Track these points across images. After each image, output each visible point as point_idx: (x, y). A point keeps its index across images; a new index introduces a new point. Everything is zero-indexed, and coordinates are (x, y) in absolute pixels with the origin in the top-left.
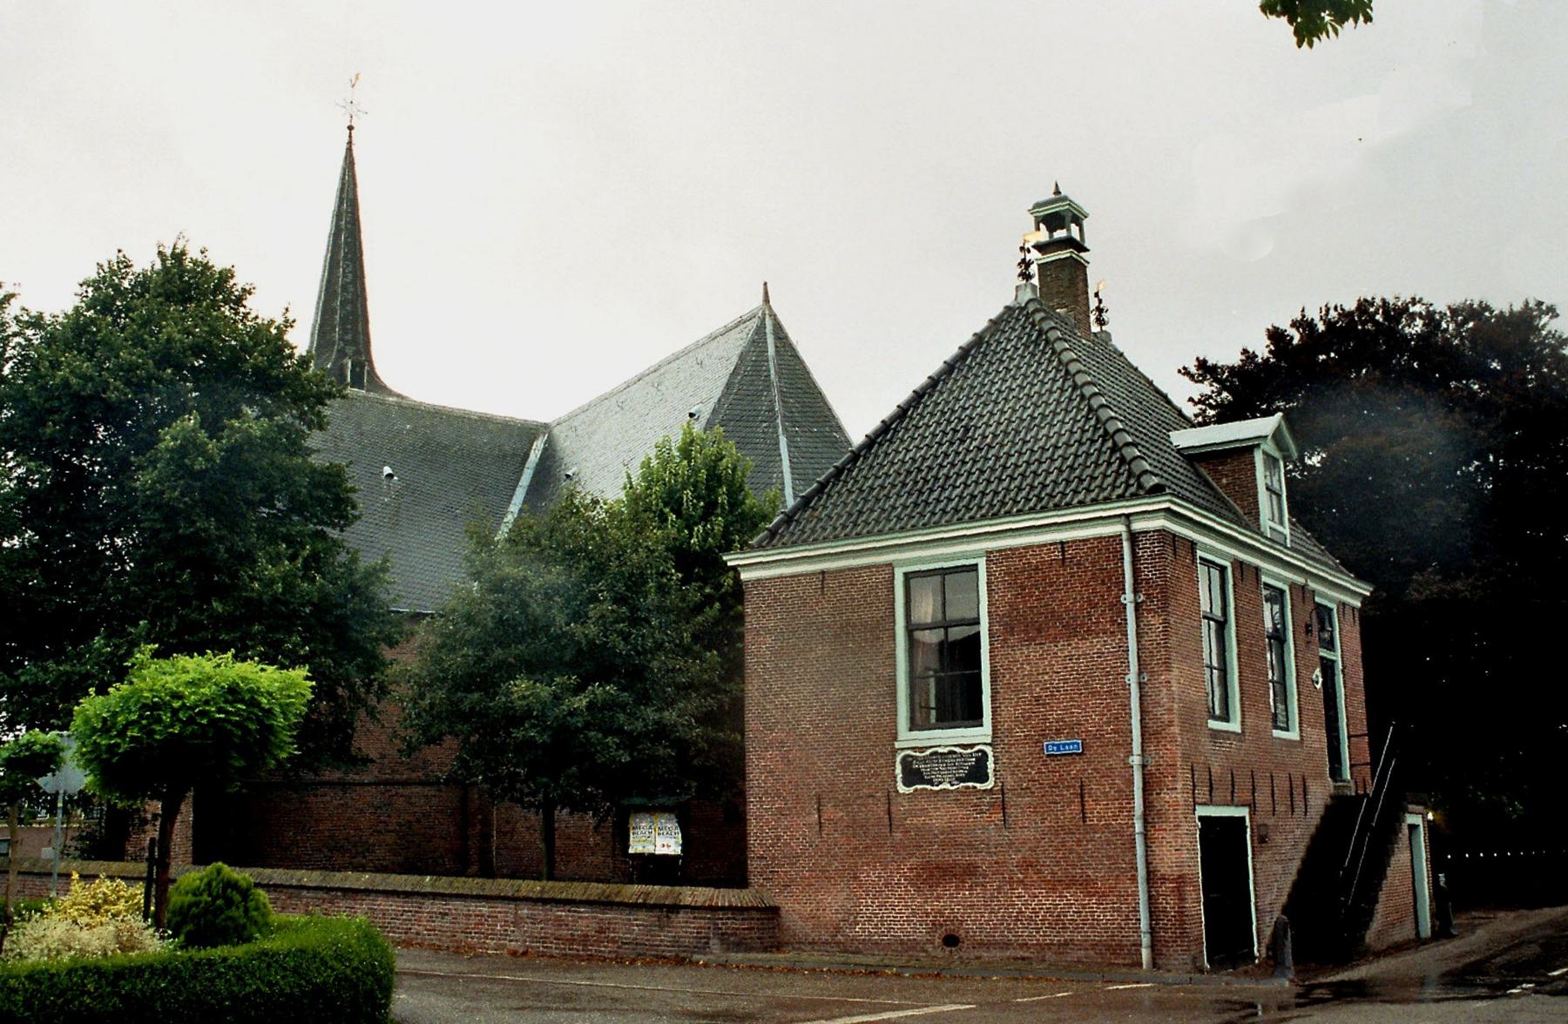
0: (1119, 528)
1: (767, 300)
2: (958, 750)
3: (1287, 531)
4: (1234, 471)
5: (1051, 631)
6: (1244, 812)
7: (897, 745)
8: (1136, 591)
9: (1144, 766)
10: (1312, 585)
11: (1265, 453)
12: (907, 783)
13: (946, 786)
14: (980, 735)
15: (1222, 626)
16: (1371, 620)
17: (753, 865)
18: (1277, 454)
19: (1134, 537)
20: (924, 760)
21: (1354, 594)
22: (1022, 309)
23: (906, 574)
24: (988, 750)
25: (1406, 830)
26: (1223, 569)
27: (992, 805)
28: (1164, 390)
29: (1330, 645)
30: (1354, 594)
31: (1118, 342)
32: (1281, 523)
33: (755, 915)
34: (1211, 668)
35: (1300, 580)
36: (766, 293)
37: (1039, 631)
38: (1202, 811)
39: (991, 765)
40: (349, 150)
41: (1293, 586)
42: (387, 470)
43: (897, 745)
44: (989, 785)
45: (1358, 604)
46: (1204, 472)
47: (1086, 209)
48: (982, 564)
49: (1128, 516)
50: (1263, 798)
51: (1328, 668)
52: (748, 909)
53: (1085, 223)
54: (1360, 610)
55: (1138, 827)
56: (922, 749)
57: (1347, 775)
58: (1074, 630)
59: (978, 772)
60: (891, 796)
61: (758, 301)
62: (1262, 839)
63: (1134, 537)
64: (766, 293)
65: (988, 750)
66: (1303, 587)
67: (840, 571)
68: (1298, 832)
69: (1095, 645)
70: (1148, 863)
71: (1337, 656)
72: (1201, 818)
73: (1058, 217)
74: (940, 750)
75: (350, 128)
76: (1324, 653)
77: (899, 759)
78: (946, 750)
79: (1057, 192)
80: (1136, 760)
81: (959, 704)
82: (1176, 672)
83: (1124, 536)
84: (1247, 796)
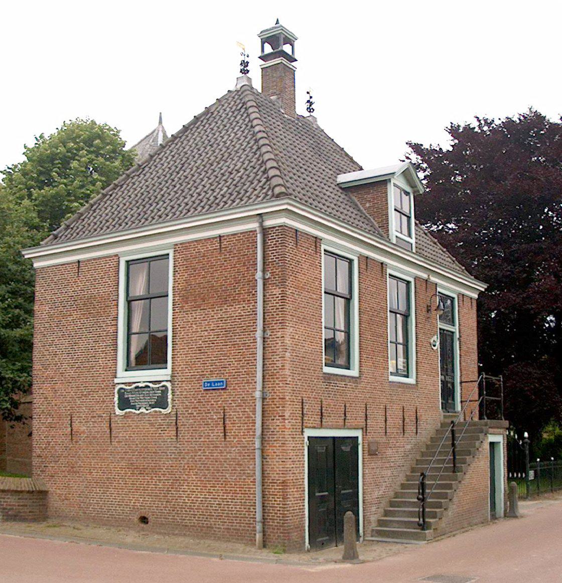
0: (254, 226)
1: (160, 122)
2: (150, 385)
3: (413, 241)
4: (374, 199)
6: (358, 433)
7: (116, 381)
8: (264, 271)
9: (264, 399)
10: (433, 279)
12: (121, 409)
13: (143, 410)
14: (161, 374)
15: (348, 300)
16: (482, 305)
17: (35, 461)
18: (408, 189)
19: (265, 231)
20: (131, 392)
22: (238, 91)
23: (127, 262)
24: (169, 385)
25: (487, 446)
27: (169, 425)
28: (351, 155)
32: (410, 235)
33: (26, 496)
34: (396, 344)
35: (425, 276)
36: (160, 118)
38: (309, 433)
39: (170, 396)
41: (416, 278)
43: (116, 381)
44: (169, 410)
45: (476, 296)
46: (356, 200)
47: (297, 35)
48: (171, 252)
50: (376, 423)
51: (446, 338)
52: (22, 492)
53: (296, 44)
54: (477, 300)
55: (257, 444)
56: (130, 384)
58: (225, 300)
59: (161, 403)
60: (111, 414)
61: (155, 125)
62: (372, 453)
63: (265, 231)
64: (160, 118)
65: (169, 385)
68: (409, 447)
69: (236, 310)
70: (263, 471)
72: (481, 418)
73: (277, 42)
74: (140, 385)
76: (441, 325)
77: (116, 390)
79: (277, 22)
80: (258, 394)
81: (152, 353)
82: (290, 330)
83: (258, 230)
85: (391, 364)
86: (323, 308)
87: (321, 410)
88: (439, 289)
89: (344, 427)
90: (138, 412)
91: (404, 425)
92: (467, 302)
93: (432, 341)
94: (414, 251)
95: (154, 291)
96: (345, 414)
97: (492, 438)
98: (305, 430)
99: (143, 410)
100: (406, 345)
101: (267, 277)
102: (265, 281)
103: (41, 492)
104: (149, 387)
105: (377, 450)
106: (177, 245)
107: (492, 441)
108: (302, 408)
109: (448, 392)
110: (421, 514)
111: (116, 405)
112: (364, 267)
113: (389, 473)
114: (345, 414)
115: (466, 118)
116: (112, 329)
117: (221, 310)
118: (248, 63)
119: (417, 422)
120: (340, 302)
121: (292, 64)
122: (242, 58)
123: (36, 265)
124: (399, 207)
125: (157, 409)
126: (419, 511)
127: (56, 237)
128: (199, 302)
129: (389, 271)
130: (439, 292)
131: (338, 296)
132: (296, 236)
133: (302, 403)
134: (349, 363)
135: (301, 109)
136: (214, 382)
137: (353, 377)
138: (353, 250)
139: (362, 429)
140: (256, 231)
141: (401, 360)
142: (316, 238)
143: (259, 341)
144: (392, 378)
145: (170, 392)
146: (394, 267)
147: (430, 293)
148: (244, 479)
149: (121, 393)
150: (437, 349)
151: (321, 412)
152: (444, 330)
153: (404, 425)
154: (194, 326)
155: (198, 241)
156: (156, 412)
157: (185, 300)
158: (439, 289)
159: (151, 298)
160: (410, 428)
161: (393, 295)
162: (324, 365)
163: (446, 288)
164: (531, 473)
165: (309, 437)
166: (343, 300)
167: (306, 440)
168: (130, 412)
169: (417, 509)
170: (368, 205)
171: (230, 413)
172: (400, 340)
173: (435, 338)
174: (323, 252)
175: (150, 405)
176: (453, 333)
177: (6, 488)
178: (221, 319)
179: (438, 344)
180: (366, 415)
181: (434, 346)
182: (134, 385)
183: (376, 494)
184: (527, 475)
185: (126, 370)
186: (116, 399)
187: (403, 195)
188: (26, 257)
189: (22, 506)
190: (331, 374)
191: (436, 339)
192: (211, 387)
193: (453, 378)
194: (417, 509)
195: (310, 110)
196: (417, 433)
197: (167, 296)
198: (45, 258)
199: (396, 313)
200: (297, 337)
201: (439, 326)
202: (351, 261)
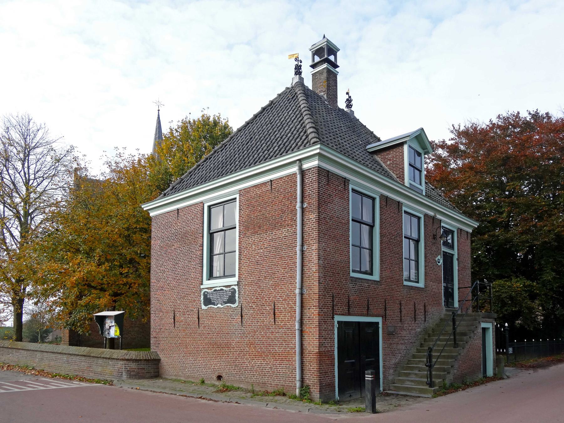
2: (224, 288)
3: (423, 187)
5: (265, 227)
6: (379, 320)
7: (202, 287)
10: (439, 217)
11: (410, 146)
12: (205, 305)
13: (219, 305)
15: (372, 227)
17: (152, 341)
19: (303, 173)
24: (236, 288)
25: (480, 331)
29: (452, 247)
31: (357, 115)
32: (421, 184)
34: (410, 260)
35: (431, 213)
37: (260, 227)
38: (337, 318)
39: (237, 295)
40: (159, 118)
41: (426, 215)
48: (237, 196)
49: (300, 160)
51: (448, 259)
52: (141, 360)
56: (211, 288)
57: (456, 305)
58: (276, 225)
59: (231, 300)
62: (389, 334)
66: (434, 218)
67: (185, 208)
68: (419, 330)
69: (284, 232)
71: (455, 252)
74: (217, 289)
75: (159, 110)
76: (444, 249)
77: (202, 293)
78: (219, 289)
83: (298, 172)
84: (382, 312)
85: (405, 274)
86: (351, 230)
87: (349, 302)
88: (442, 224)
89: (368, 315)
90: (216, 307)
91: (415, 315)
92: (464, 235)
94: (424, 194)
95: (227, 226)
96: (368, 306)
97: (483, 325)
98: (335, 316)
99: (219, 305)
100: (417, 261)
101: (305, 206)
102: (303, 210)
103: (155, 360)
105: (394, 332)
106: (241, 190)
108: (333, 301)
109: (449, 295)
110: (429, 376)
111: (202, 303)
113: (404, 347)
114: (368, 306)
115: (463, 124)
116: (199, 253)
117: (272, 233)
118: (301, 66)
119: (425, 313)
120: (365, 229)
121: (337, 69)
122: (297, 63)
123: (152, 214)
124: (413, 163)
126: (427, 374)
127: (165, 195)
128: (257, 229)
129: (404, 208)
132: (328, 176)
133: (333, 297)
135: (342, 104)
137: (375, 281)
138: (376, 191)
139: (383, 317)
140: (296, 173)
141: (413, 271)
142: (345, 178)
143: (298, 253)
144: (406, 283)
145: (237, 292)
146: (407, 205)
147: (436, 226)
148: (288, 351)
149: (205, 295)
151: (349, 304)
153: (415, 315)
154: (253, 246)
155: (255, 186)
156: (228, 306)
158: (442, 224)
159: (225, 230)
160: (421, 317)
161: (408, 227)
162: (351, 271)
163: (447, 223)
164: (511, 350)
166: (368, 227)
168: (211, 307)
169: (426, 373)
170: (389, 163)
171: (279, 305)
172: (413, 257)
173: (439, 257)
175: (224, 302)
176: (453, 255)
177: (130, 358)
178: (272, 240)
179: (441, 261)
181: (439, 262)
182: (214, 289)
183: (393, 361)
184: (507, 350)
185: (209, 280)
186: (202, 298)
188: (145, 209)
190: (357, 278)
191: (440, 259)
193: (453, 285)
194: (426, 373)
196: (425, 321)
197: (235, 228)
198: (157, 209)
199: (409, 239)
200: (328, 250)
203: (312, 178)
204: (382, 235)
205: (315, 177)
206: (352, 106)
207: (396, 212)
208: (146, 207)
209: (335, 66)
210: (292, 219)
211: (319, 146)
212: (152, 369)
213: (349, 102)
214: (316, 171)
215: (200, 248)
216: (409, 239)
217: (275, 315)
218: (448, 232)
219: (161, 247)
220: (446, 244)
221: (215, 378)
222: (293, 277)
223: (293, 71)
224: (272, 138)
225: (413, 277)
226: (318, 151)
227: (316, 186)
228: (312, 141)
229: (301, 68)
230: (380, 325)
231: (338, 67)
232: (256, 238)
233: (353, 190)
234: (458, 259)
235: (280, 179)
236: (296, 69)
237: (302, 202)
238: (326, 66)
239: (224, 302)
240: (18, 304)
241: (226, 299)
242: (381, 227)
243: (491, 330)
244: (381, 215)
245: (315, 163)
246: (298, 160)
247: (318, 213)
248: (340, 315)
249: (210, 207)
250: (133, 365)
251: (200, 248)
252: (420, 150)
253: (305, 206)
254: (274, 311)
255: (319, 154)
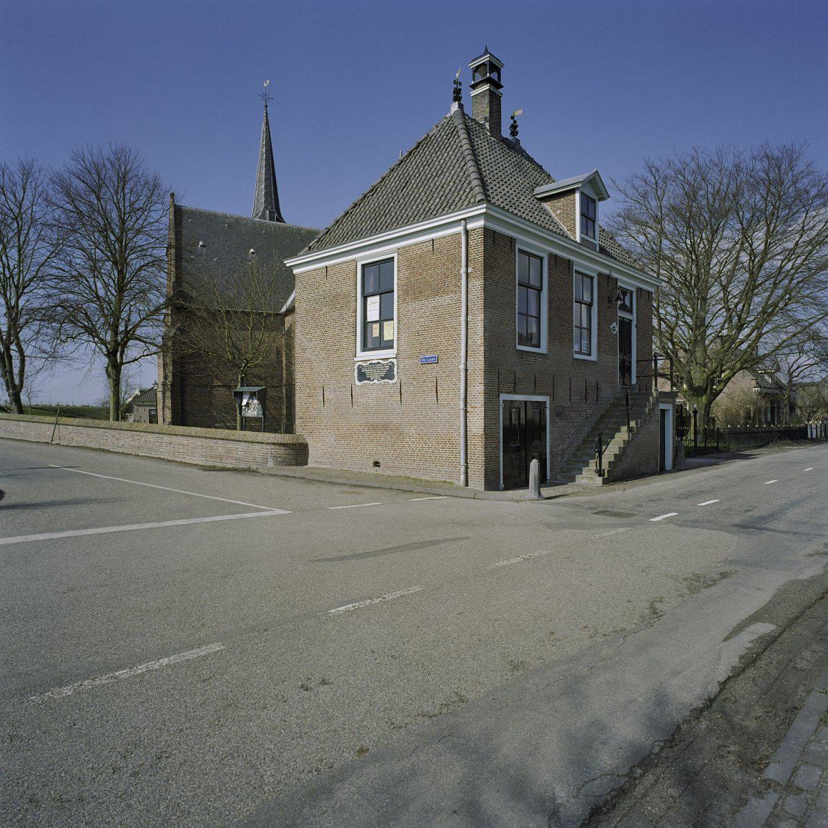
2: (381, 362)
7: (356, 359)
10: (615, 275)
15: (539, 290)
19: (467, 232)
21: (483, 208)
23: (363, 266)
24: (394, 361)
26: (592, 278)
29: (630, 311)
30: (483, 208)
32: (594, 238)
34: (581, 328)
35: (606, 272)
38: (503, 397)
41: (600, 275)
42: (252, 250)
43: (356, 359)
44: (395, 380)
48: (395, 255)
57: (634, 381)
58: (438, 291)
59: (389, 375)
66: (608, 277)
69: (446, 300)
74: (374, 362)
75: (266, 106)
76: (621, 314)
78: (376, 362)
85: (576, 348)
86: (517, 297)
88: (619, 284)
90: (371, 383)
93: (611, 327)
97: (662, 406)
99: (376, 381)
104: (380, 363)
107: (662, 408)
111: (356, 378)
112: (554, 264)
116: (352, 320)
118: (460, 90)
121: (500, 90)
122: (455, 86)
123: (295, 271)
125: (386, 380)
128: (418, 294)
129: (575, 268)
130: (619, 287)
131: (530, 288)
134: (539, 343)
136: (429, 358)
140: (460, 233)
141: (585, 342)
143: (463, 323)
144: (576, 356)
146: (580, 264)
149: (360, 368)
150: (616, 334)
152: (623, 318)
157: (406, 293)
165: (503, 400)
167: (502, 405)
170: (558, 212)
172: (585, 325)
174: (517, 250)
175: (381, 377)
176: (631, 320)
178: (434, 308)
179: (617, 329)
180: (553, 384)
181: (614, 330)
182: (369, 362)
185: (363, 351)
187: (590, 201)
188: (287, 265)
189: (462, 539)
191: (615, 326)
192: (426, 362)
193: (631, 357)
195: (514, 133)
201: (619, 315)
202: (541, 259)
203: (478, 243)
204: (550, 301)
205: (481, 239)
206: (517, 133)
207: (566, 272)
208: (289, 263)
209: (499, 86)
210: (456, 285)
211: (485, 205)
212: (299, 453)
213: (514, 128)
214: (481, 231)
215: (353, 314)
216: (581, 303)
217: (437, 392)
218: (625, 292)
219: (307, 312)
220: (623, 307)
221: (371, 465)
222: (457, 350)
223: (452, 96)
224: (419, 161)
225: (584, 349)
226: (484, 210)
227: (481, 248)
228: (478, 199)
229: (460, 93)
230: (548, 405)
231: (501, 87)
232: (416, 305)
233: (519, 250)
234: (636, 326)
235: (442, 238)
236: (454, 92)
237: (467, 266)
238: (488, 88)
239: (381, 377)
240: (115, 368)
241: (383, 374)
242: (550, 292)
243: (671, 412)
244: (550, 277)
245: (481, 223)
246: (462, 219)
247: (484, 280)
248: (505, 393)
249: (363, 266)
250: (281, 451)
251: (353, 314)
252: (594, 196)
253: (469, 271)
254: (437, 388)
255: (485, 213)
